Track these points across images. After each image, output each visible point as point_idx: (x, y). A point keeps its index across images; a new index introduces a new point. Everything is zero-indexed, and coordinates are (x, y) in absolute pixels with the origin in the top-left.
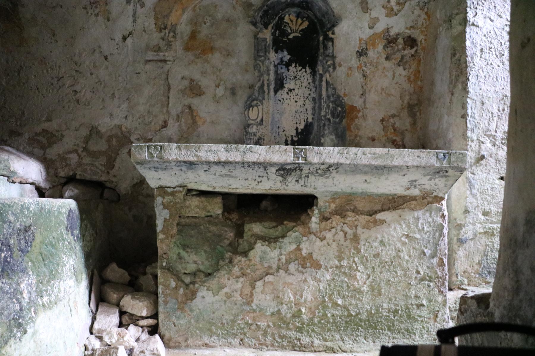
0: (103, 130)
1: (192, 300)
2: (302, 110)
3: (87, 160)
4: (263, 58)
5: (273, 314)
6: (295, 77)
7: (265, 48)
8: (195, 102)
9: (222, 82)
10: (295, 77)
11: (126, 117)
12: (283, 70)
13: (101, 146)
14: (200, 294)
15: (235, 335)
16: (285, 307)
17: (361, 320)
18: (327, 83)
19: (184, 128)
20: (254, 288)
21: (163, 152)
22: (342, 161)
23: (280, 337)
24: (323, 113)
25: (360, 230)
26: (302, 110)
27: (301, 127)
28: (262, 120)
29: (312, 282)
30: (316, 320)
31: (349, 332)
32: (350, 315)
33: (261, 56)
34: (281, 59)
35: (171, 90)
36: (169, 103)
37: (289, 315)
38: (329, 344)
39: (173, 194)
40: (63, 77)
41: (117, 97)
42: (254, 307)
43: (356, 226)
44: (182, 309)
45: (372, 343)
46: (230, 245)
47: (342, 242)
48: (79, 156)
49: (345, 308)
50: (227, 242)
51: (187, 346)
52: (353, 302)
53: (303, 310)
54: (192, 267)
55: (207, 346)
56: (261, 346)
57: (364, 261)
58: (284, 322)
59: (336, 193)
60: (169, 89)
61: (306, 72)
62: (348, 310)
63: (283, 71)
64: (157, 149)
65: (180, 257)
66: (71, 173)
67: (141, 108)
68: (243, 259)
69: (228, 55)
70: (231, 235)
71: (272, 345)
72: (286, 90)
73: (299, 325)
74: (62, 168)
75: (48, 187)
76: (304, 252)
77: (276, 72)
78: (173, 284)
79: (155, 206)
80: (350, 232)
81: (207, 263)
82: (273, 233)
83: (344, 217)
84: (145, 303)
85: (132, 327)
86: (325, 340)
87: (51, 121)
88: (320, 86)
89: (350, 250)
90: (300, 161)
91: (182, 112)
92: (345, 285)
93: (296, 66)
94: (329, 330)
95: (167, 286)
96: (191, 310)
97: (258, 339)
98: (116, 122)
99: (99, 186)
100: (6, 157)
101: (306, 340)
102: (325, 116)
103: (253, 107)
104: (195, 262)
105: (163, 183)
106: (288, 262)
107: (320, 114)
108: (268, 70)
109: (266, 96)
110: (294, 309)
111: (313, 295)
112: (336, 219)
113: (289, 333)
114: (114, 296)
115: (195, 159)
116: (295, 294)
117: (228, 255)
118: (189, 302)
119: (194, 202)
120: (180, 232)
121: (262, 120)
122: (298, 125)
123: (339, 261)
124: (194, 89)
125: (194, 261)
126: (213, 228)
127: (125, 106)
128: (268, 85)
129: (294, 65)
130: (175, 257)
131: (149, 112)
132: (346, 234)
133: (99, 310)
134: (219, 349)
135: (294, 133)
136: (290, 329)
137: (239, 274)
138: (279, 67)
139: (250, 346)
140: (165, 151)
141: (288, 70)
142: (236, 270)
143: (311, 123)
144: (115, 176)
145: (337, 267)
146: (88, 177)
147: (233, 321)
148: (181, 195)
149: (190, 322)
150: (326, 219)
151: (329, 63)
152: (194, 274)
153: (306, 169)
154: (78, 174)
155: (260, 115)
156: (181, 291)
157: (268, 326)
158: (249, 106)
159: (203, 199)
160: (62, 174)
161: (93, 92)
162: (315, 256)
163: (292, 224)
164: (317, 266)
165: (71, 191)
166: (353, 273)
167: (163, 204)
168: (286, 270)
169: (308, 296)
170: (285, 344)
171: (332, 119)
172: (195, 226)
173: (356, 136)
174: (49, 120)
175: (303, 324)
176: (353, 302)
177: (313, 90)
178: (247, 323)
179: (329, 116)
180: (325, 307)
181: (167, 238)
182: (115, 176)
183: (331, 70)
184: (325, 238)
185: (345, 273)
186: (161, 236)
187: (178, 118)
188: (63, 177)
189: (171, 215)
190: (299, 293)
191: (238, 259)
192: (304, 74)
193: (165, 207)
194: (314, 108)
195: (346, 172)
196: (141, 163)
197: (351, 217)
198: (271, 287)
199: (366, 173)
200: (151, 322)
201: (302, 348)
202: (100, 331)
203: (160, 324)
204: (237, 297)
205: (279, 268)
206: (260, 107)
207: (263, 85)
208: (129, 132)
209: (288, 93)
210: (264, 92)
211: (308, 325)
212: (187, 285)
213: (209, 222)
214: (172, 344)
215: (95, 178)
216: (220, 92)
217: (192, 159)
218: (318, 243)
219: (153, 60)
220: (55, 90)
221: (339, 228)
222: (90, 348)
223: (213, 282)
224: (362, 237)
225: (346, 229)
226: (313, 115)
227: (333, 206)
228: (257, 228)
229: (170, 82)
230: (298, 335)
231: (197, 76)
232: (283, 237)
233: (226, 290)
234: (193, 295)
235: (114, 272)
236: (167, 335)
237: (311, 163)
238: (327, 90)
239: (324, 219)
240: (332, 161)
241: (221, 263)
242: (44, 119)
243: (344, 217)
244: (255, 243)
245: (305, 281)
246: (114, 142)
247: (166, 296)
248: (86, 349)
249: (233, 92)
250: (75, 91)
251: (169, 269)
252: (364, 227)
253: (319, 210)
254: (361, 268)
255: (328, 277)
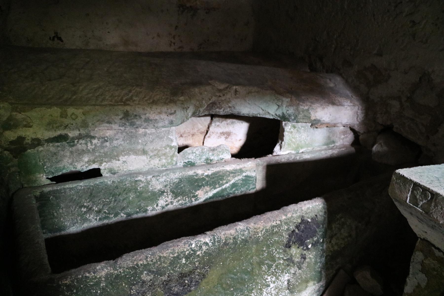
21: (433, 204)
40: (401, 2)
64: (426, 197)
66: (389, 123)
74: (382, 114)
75: (362, 132)
79: (412, 260)
87: (381, 55)
100: (306, 108)
140: (436, 205)
154: (395, 126)
160: (380, 121)
161: (436, 25)
165: (380, 146)
167: (422, 264)
174: (380, 54)
188: (382, 125)
220: (391, 19)
242: (375, 52)
250: (413, 22)
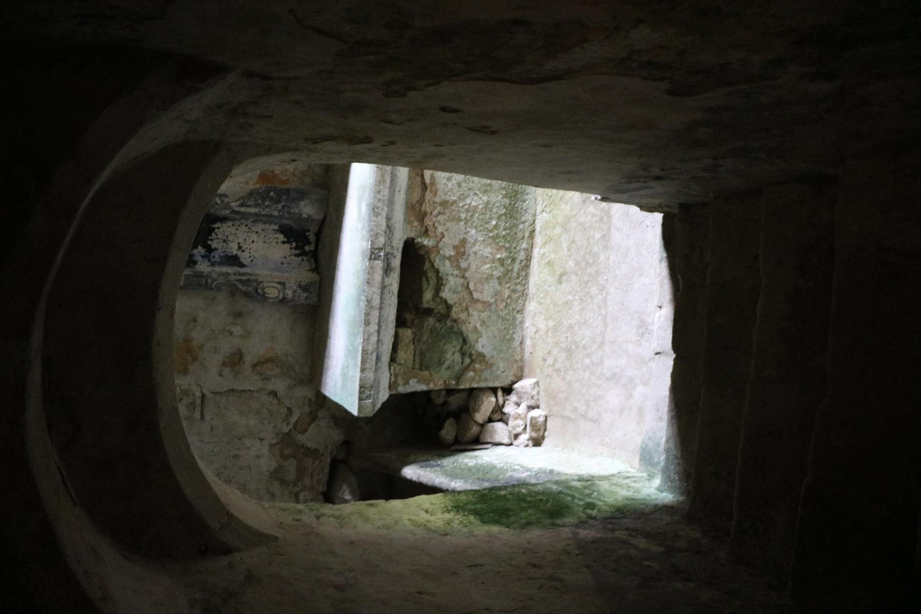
0: (275, 464)
1: (484, 356)
2: (262, 236)
3: (307, 481)
4: (209, 281)
5: (500, 284)
6: (224, 241)
7: (198, 277)
8: (249, 359)
9: (227, 328)
10: (224, 241)
11: (261, 440)
12: (216, 256)
13: (291, 466)
14: (480, 349)
15: (514, 318)
16: (495, 272)
17: (510, 204)
18: (242, 205)
19: (277, 371)
20: (478, 300)
22: (384, 215)
23: (518, 278)
24: (276, 213)
25: (437, 200)
26: (262, 236)
27: (281, 237)
28: (280, 283)
29: (477, 247)
30: (507, 245)
31: (518, 215)
32: (505, 214)
33: (206, 282)
34: (202, 257)
35: (235, 388)
36: (250, 391)
37: (502, 269)
38: (527, 235)
39: (396, 376)
41: (237, 452)
42: (493, 300)
43: (434, 203)
44: (492, 365)
45: (529, 196)
46: (439, 321)
47: (445, 217)
48: (301, 490)
49: (499, 218)
50: (438, 324)
51: (522, 360)
52: (495, 210)
53: (499, 256)
54: (458, 357)
55: (521, 343)
56: (524, 295)
57: (463, 197)
58: (507, 274)
59: (405, 219)
60: (233, 390)
61: (218, 228)
62: (501, 215)
63: (217, 256)
65: (449, 368)
67: (252, 422)
68: (454, 309)
69: (195, 321)
70: (431, 321)
71: (524, 285)
72: (239, 253)
73: (510, 261)
76: (453, 253)
77: (221, 264)
78: (471, 374)
80: (438, 209)
81: (454, 343)
82: (433, 281)
83: (425, 214)
84: (485, 399)
85: (506, 410)
86: (523, 237)
88: (244, 213)
89: (453, 210)
90: (382, 254)
91: (260, 374)
92: (481, 217)
93: (212, 240)
94: (516, 234)
95: (473, 379)
96: (493, 357)
97: (519, 297)
98: (265, 450)
99: (334, 463)
101: (522, 255)
102: (279, 211)
103: (264, 293)
104: (453, 354)
105: (387, 385)
106: (459, 267)
107: (276, 217)
108: (222, 274)
109: (254, 278)
110: (497, 264)
111: (487, 247)
112: (428, 222)
113: (516, 270)
114: (475, 429)
115: (375, 354)
116: (485, 263)
117: (449, 323)
118: (487, 359)
119: (402, 355)
120: (427, 369)
121: (280, 283)
122: (279, 241)
123: (461, 220)
124: (235, 360)
125: (452, 355)
126: (425, 338)
127: (248, 442)
128: (242, 274)
129: (209, 242)
130: (449, 373)
131: (257, 413)
132: (439, 213)
133: (489, 440)
134: (525, 332)
135: (287, 246)
136: (512, 269)
137: (466, 313)
138: (213, 260)
139: (524, 305)
141: (216, 249)
142: (463, 316)
143: (280, 226)
144: (326, 447)
145: (466, 223)
146: (325, 478)
147: (503, 319)
148: (398, 368)
149: (502, 358)
150: (426, 231)
151: (219, 202)
152: (463, 354)
153: (388, 249)
155: (274, 285)
156: (477, 366)
157: (509, 288)
158: (264, 297)
159: (399, 347)
162: (456, 244)
163: (427, 263)
164: (464, 241)
166: (471, 209)
167: (405, 384)
168: (466, 270)
169: (487, 251)
170: (524, 274)
171: (283, 203)
172: (422, 353)
173: (294, 175)
175: (509, 257)
176: (495, 210)
177: (243, 221)
178: (506, 307)
179: (280, 207)
180: (498, 236)
181: (433, 380)
182: (326, 447)
183: (226, 200)
184: (442, 233)
185: (472, 216)
186: (431, 386)
187: (267, 379)
189: (414, 377)
190: (484, 260)
191: (453, 315)
192: (221, 230)
193: (406, 383)
194: (265, 223)
195: (392, 210)
196: (374, 407)
197: (426, 207)
198: (478, 284)
199: (394, 191)
200: (500, 393)
201: (529, 259)
202: (510, 438)
203: (503, 385)
204: (484, 315)
205: (463, 277)
206: (265, 285)
207: (241, 281)
208: (277, 435)
209: (243, 251)
210: (249, 279)
211: (510, 252)
212: (472, 362)
213: (419, 340)
214: (519, 375)
215: (327, 470)
216: (237, 330)
217: (374, 357)
218: (445, 239)
219: (202, 411)
221: (434, 219)
222: (526, 443)
223: (471, 337)
224: (443, 197)
225: (435, 212)
226: (271, 223)
227: (416, 224)
228: (428, 295)
229: (225, 389)
230: (518, 262)
231: (219, 358)
232: (437, 272)
233: (478, 326)
234: (481, 356)
235: (448, 432)
236: (511, 378)
237: (385, 244)
238: (249, 206)
239: (426, 233)
240: (384, 224)
241: (455, 329)
243: (425, 214)
244: (441, 298)
245: (475, 253)
246: (287, 451)
247: (480, 380)
248: (527, 446)
249: (238, 315)
251: (458, 378)
252: (436, 195)
253: (418, 236)
254: (468, 201)
255: (473, 232)
